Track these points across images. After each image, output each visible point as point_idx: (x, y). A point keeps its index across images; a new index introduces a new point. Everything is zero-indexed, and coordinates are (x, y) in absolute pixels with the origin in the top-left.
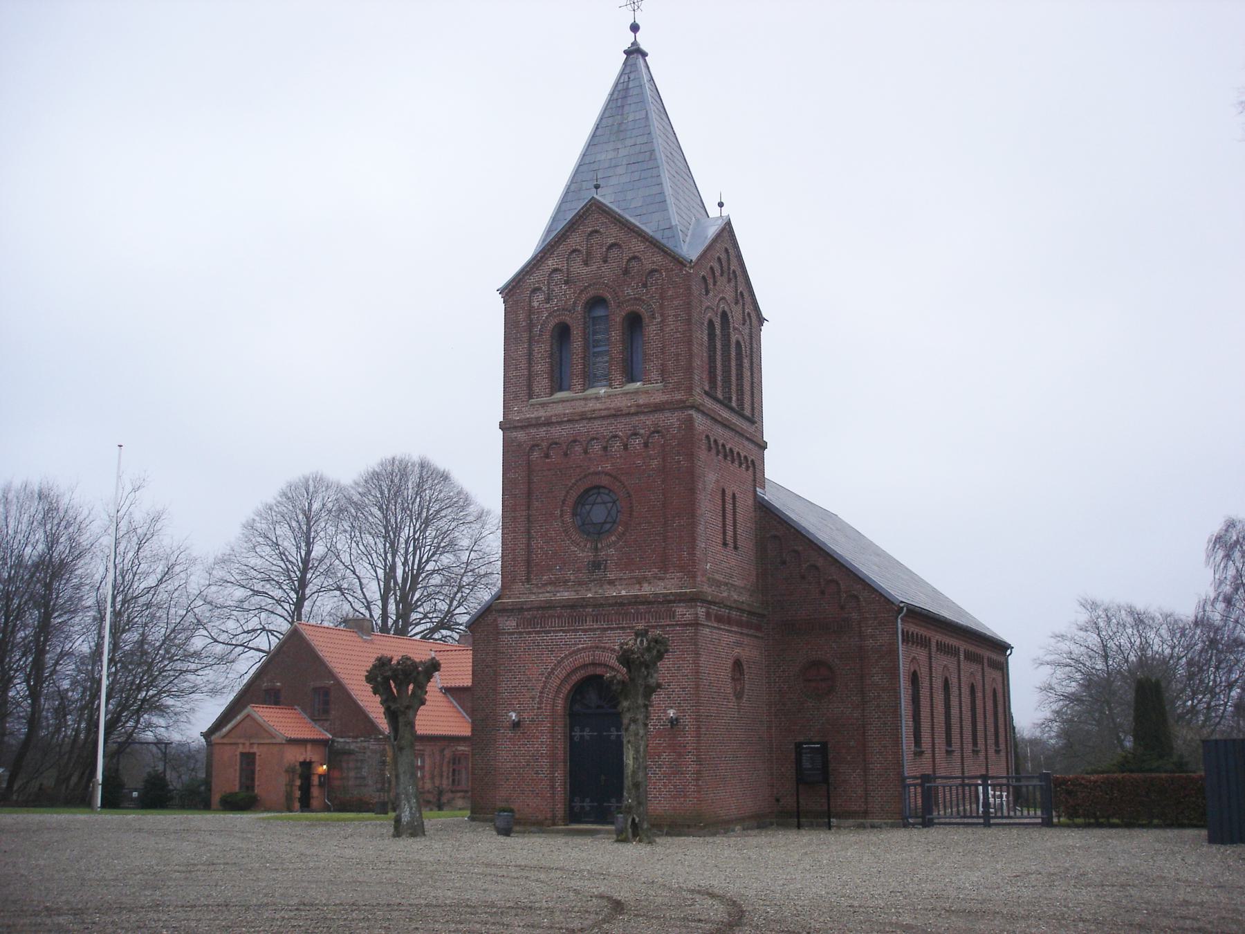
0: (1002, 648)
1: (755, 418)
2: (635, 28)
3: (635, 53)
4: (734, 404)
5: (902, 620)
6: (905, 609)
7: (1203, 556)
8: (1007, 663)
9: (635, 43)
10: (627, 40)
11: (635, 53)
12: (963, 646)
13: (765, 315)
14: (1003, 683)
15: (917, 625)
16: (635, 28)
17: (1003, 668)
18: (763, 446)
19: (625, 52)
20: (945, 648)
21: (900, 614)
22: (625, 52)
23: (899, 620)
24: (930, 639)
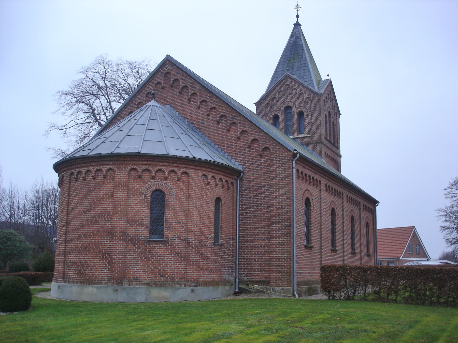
0: (374, 202)
1: (338, 147)
2: (298, 16)
3: (297, 25)
4: (332, 142)
5: (296, 163)
6: (298, 155)
7: (447, 185)
8: (375, 210)
9: (297, 22)
10: (296, 19)
11: (297, 25)
12: (362, 202)
13: (413, 226)
14: (373, 221)
15: (304, 167)
16: (298, 16)
17: (373, 213)
18: (341, 157)
19: (294, 24)
20: (354, 202)
21: (294, 158)
22: (294, 24)
23: (294, 162)
24: (360, 203)
